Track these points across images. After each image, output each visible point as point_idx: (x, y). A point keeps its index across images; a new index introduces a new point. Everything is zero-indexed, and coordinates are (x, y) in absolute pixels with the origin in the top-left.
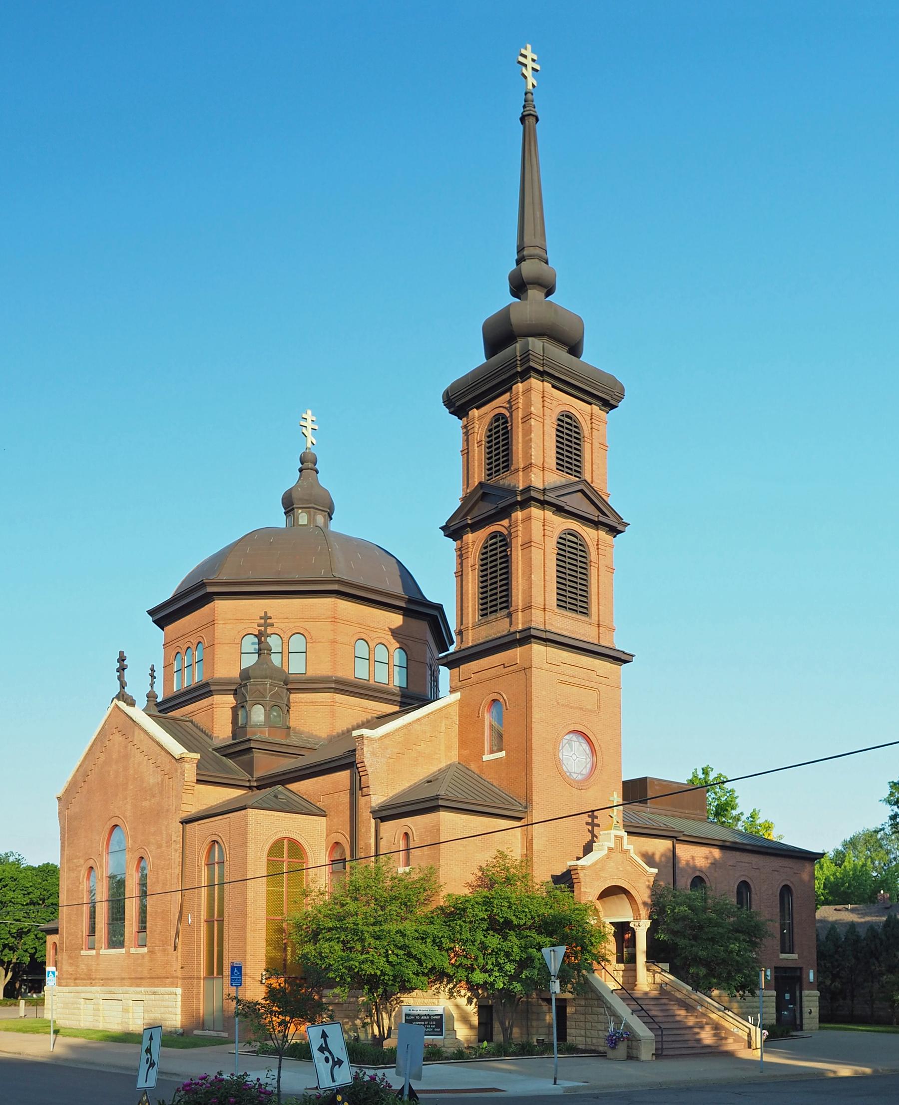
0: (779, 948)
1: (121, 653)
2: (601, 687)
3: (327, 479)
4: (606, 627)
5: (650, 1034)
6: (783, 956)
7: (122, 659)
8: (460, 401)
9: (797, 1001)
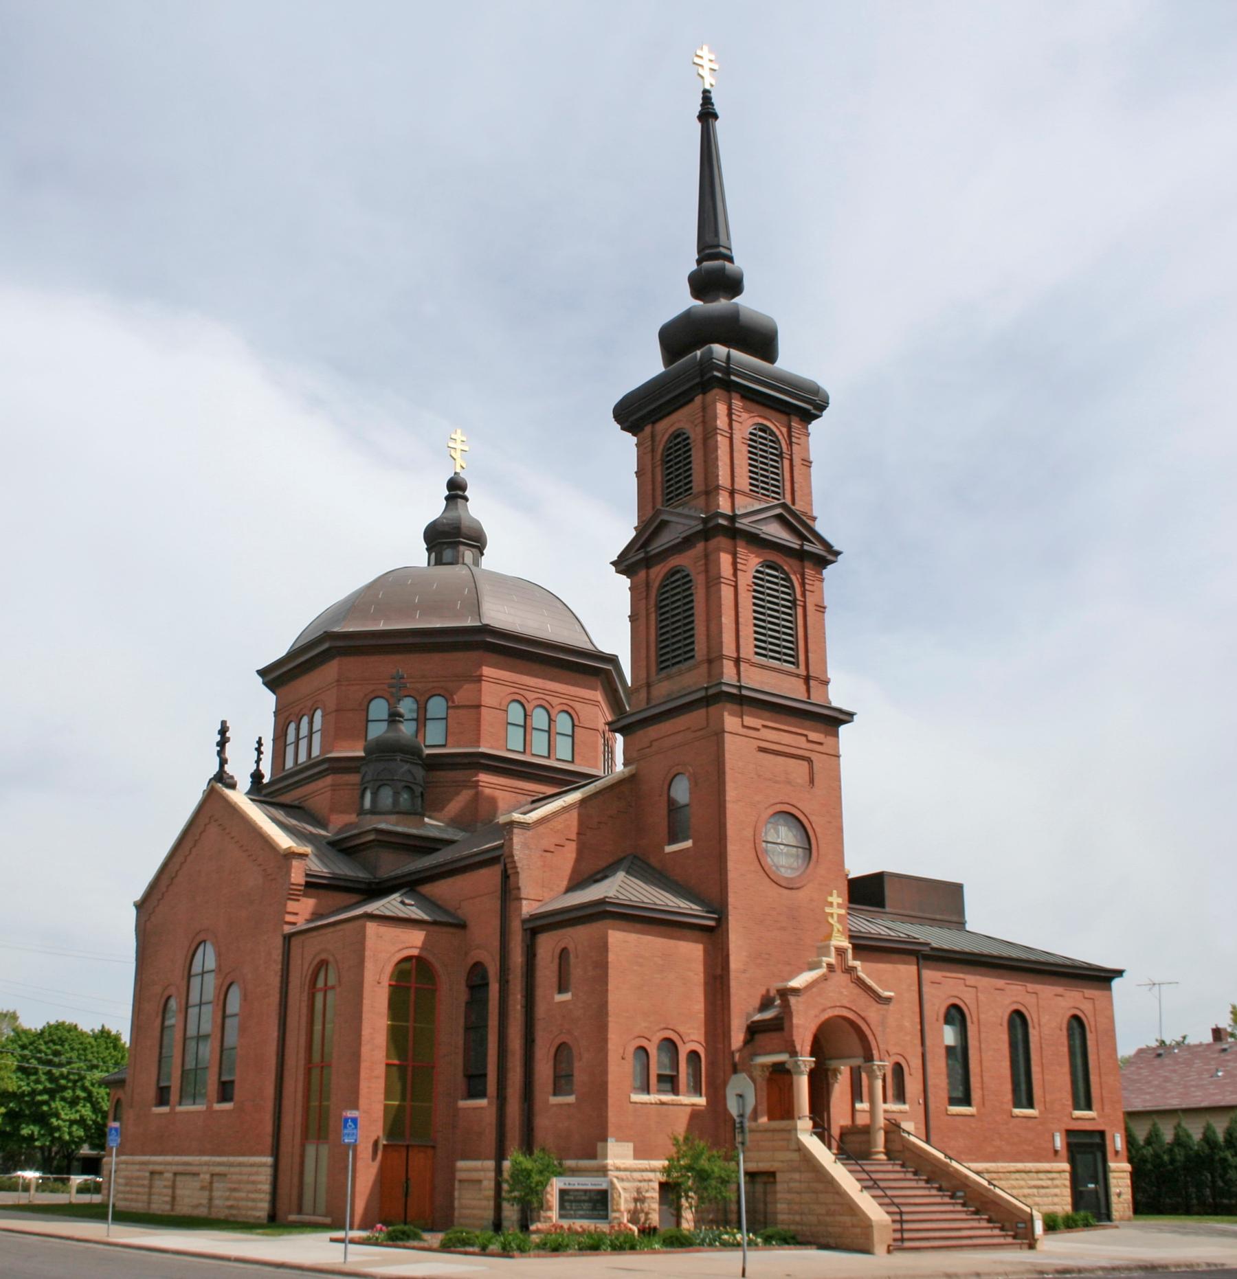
0: (1070, 1102)
1: (224, 723)
2: (814, 756)
3: (478, 508)
4: (816, 679)
6: (1077, 1113)
7: (223, 731)
8: (634, 413)
9: (1102, 1177)
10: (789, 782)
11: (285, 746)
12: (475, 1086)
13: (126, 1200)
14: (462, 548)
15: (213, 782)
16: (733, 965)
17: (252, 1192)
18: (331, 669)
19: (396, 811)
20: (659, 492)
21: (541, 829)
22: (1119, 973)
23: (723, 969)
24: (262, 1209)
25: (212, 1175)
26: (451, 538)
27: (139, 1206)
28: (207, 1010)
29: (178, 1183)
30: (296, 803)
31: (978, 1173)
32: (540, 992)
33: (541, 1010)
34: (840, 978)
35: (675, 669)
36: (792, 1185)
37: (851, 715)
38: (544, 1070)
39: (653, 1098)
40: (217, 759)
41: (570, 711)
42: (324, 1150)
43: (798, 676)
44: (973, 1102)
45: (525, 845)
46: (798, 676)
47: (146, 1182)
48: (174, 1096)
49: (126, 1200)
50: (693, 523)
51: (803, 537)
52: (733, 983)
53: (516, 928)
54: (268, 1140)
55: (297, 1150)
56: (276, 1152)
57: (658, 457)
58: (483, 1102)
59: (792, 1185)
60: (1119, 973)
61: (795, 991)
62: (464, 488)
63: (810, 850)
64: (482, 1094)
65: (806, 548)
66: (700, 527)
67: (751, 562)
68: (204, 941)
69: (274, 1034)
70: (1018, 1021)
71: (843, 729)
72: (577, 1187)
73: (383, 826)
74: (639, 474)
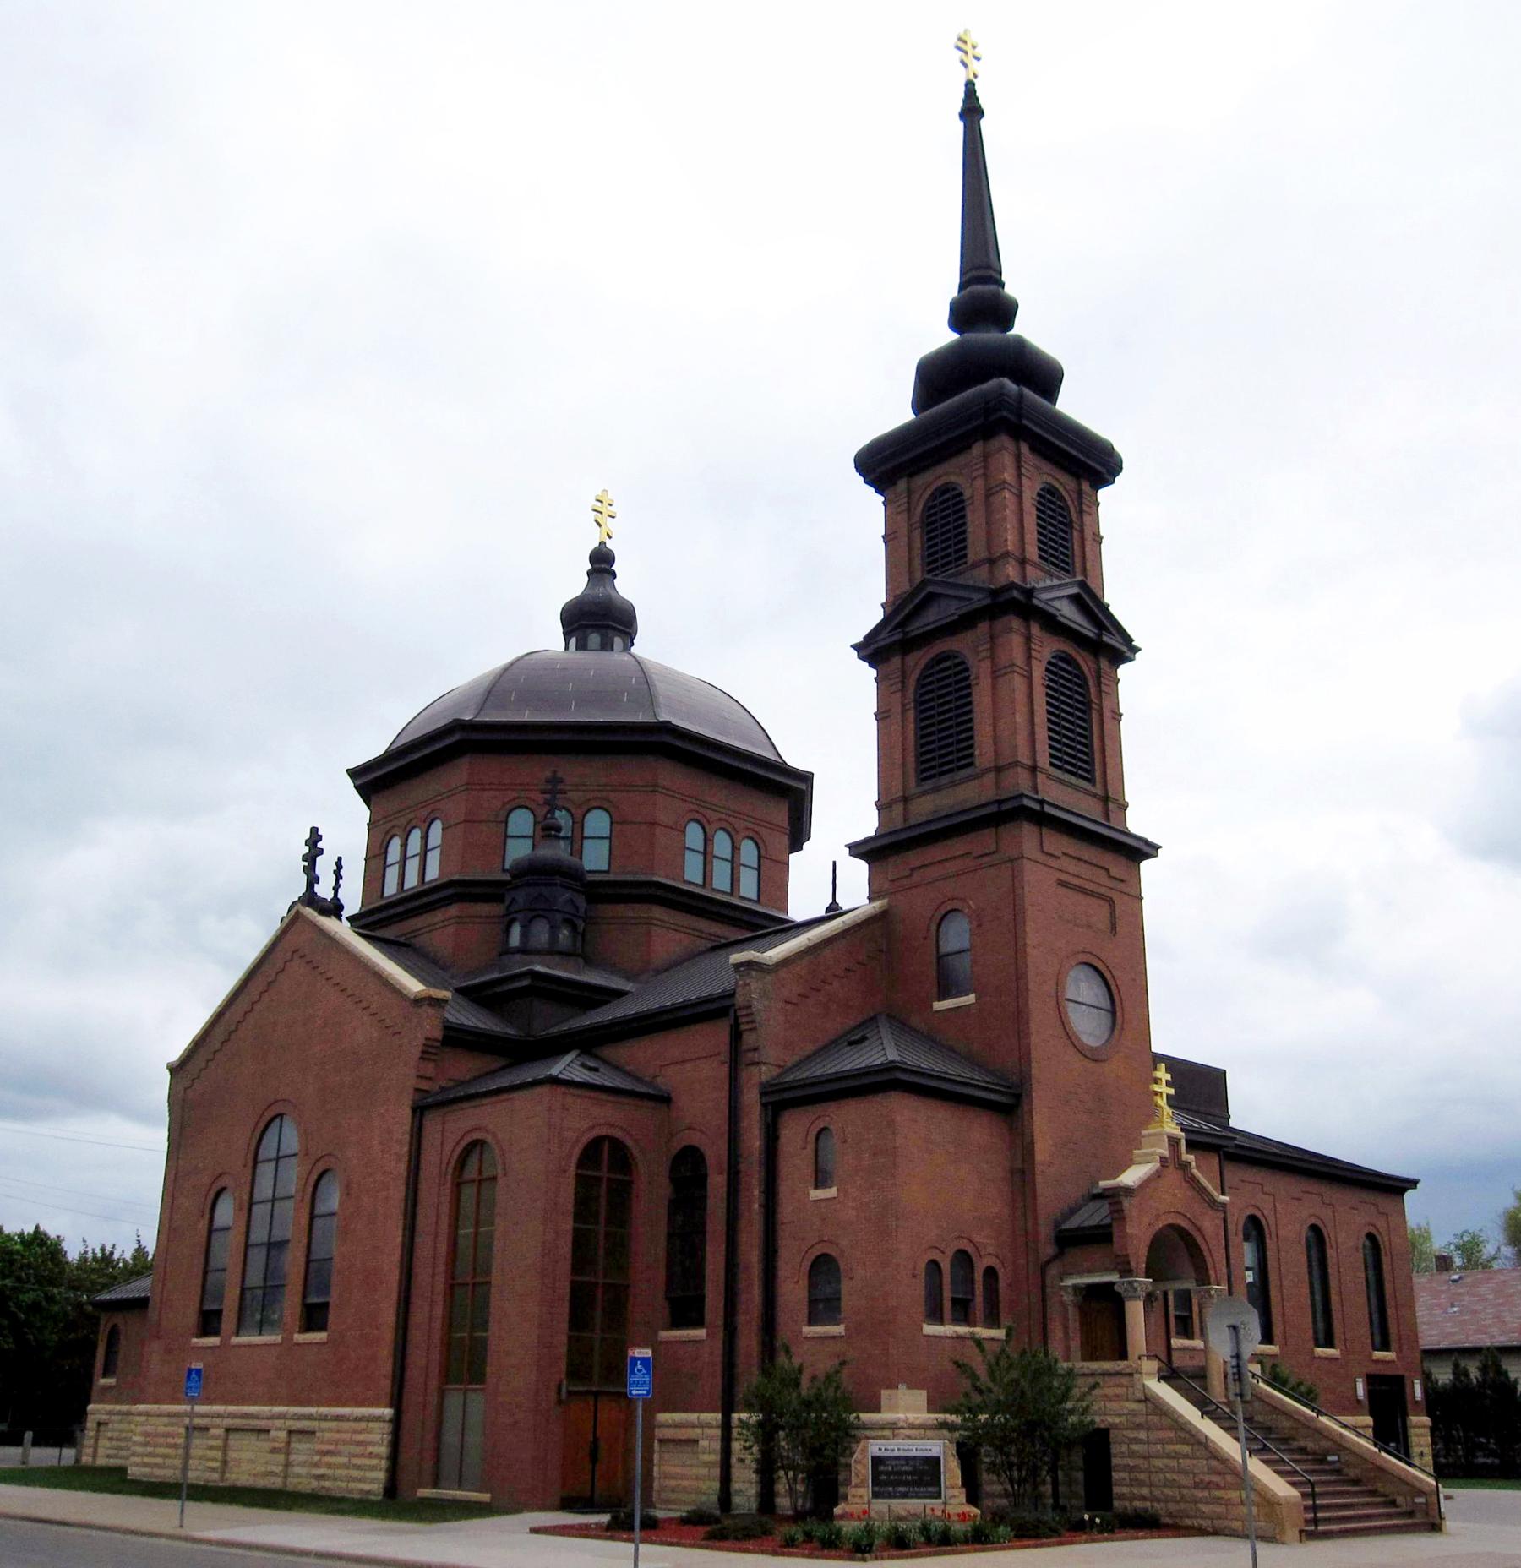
1: (314, 830)
2: (1115, 896)
3: (627, 585)
5: (1293, 1493)
8: (882, 464)
10: (1089, 926)
11: (385, 867)
12: (686, 1311)
13: (146, 1465)
14: (611, 633)
15: (299, 907)
16: (1039, 1157)
17: (356, 1456)
18: (459, 772)
19: (552, 951)
20: (917, 562)
21: (783, 973)
22: (1413, 1183)
23: (1023, 1161)
24: (374, 1481)
25: (290, 1432)
26: (599, 618)
27: (168, 1474)
28: (287, 1209)
29: (231, 1443)
30: (402, 939)
31: (1345, 1426)
32: (784, 1188)
33: (786, 1210)
34: (1173, 1175)
35: (945, 780)
36: (1135, 1447)
37: (1156, 848)
38: (793, 1291)
39: (948, 1330)
40: (318, 871)
41: (756, 837)
42: (477, 1402)
43: (1095, 795)
44: (1336, 1342)
45: (764, 994)
46: (1095, 795)
47: (181, 1441)
48: (228, 1321)
49: (146, 1465)
50: (976, 596)
51: (1100, 626)
52: (1039, 1179)
53: (751, 1098)
54: (386, 1385)
55: (433, 1399)
56: (397, 1402)
57: (917, 518)
58: (700, 1333)
59: (1135, 1447)
60: (1413, 1183)
61: (1128, 1191)
62: (612, 561)
63: (1113, 1013)
64: (698, 1322)
65: (1105, 639)
66: (988, 601)
67: (1047, 647)
68: (281, 1115)
69: (398, 1237)
70: (1317, 1238)
71: (1145, 866)
72: (896, 1453)
73: (538, 968)
74: (888, 538)
